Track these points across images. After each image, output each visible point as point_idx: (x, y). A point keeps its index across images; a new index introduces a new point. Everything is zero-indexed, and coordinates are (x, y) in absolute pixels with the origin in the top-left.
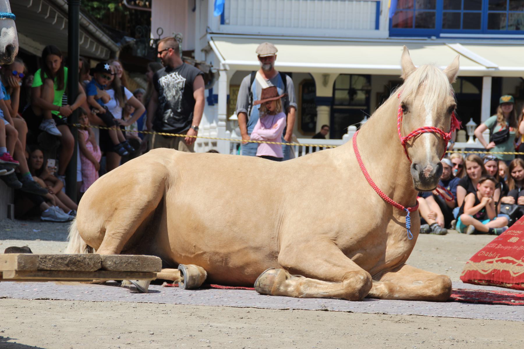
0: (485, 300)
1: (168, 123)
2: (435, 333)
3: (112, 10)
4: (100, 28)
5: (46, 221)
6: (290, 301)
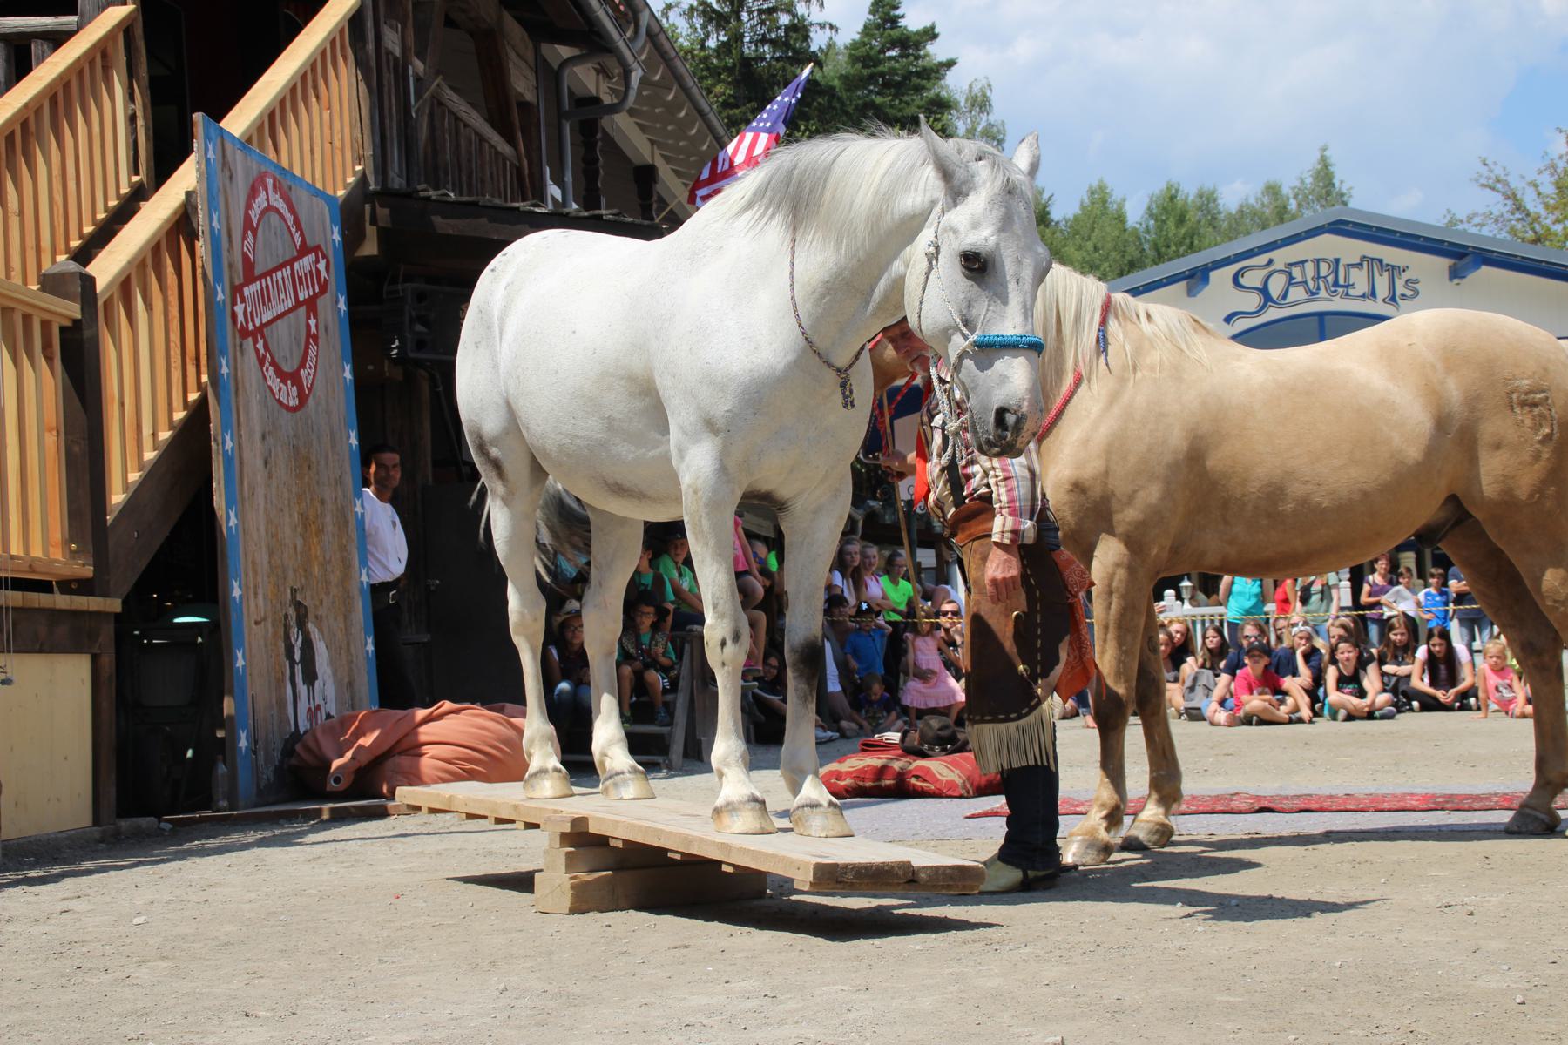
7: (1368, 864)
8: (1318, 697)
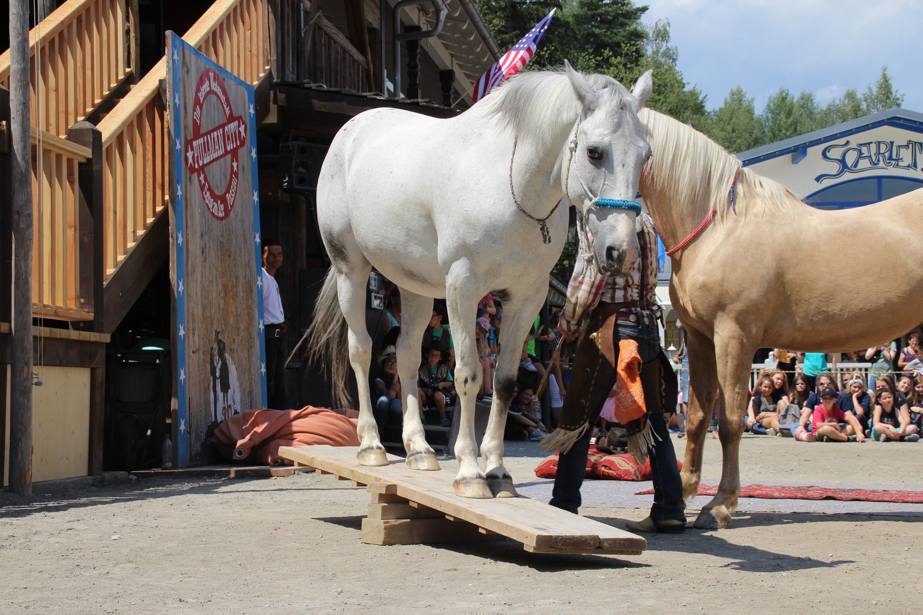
0: (908, 500)
1: (906, 353)
2: (870, 529)
3: (567, 266)
4: (561, 282)
5: (534, 441)
6: (69, 522)
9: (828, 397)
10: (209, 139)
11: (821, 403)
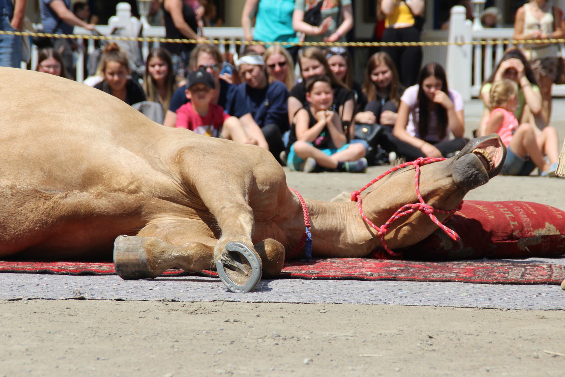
2: (251, 327)
7: (294, 341)
8: (282, 143)
9: (201, 86)
10: (561, 171)
11: (187, 101)
